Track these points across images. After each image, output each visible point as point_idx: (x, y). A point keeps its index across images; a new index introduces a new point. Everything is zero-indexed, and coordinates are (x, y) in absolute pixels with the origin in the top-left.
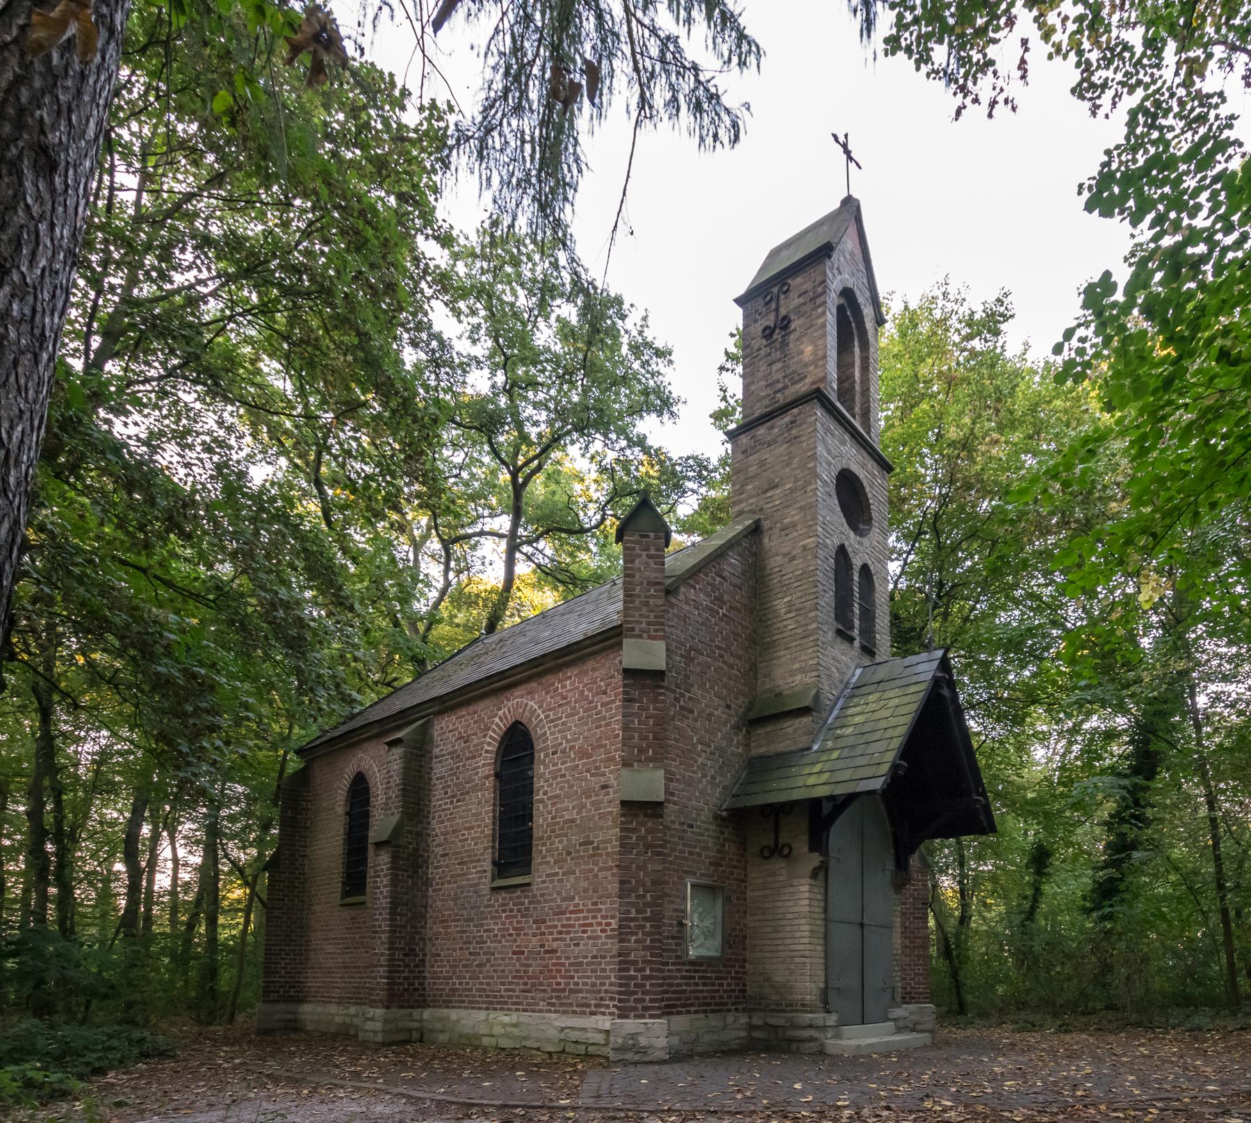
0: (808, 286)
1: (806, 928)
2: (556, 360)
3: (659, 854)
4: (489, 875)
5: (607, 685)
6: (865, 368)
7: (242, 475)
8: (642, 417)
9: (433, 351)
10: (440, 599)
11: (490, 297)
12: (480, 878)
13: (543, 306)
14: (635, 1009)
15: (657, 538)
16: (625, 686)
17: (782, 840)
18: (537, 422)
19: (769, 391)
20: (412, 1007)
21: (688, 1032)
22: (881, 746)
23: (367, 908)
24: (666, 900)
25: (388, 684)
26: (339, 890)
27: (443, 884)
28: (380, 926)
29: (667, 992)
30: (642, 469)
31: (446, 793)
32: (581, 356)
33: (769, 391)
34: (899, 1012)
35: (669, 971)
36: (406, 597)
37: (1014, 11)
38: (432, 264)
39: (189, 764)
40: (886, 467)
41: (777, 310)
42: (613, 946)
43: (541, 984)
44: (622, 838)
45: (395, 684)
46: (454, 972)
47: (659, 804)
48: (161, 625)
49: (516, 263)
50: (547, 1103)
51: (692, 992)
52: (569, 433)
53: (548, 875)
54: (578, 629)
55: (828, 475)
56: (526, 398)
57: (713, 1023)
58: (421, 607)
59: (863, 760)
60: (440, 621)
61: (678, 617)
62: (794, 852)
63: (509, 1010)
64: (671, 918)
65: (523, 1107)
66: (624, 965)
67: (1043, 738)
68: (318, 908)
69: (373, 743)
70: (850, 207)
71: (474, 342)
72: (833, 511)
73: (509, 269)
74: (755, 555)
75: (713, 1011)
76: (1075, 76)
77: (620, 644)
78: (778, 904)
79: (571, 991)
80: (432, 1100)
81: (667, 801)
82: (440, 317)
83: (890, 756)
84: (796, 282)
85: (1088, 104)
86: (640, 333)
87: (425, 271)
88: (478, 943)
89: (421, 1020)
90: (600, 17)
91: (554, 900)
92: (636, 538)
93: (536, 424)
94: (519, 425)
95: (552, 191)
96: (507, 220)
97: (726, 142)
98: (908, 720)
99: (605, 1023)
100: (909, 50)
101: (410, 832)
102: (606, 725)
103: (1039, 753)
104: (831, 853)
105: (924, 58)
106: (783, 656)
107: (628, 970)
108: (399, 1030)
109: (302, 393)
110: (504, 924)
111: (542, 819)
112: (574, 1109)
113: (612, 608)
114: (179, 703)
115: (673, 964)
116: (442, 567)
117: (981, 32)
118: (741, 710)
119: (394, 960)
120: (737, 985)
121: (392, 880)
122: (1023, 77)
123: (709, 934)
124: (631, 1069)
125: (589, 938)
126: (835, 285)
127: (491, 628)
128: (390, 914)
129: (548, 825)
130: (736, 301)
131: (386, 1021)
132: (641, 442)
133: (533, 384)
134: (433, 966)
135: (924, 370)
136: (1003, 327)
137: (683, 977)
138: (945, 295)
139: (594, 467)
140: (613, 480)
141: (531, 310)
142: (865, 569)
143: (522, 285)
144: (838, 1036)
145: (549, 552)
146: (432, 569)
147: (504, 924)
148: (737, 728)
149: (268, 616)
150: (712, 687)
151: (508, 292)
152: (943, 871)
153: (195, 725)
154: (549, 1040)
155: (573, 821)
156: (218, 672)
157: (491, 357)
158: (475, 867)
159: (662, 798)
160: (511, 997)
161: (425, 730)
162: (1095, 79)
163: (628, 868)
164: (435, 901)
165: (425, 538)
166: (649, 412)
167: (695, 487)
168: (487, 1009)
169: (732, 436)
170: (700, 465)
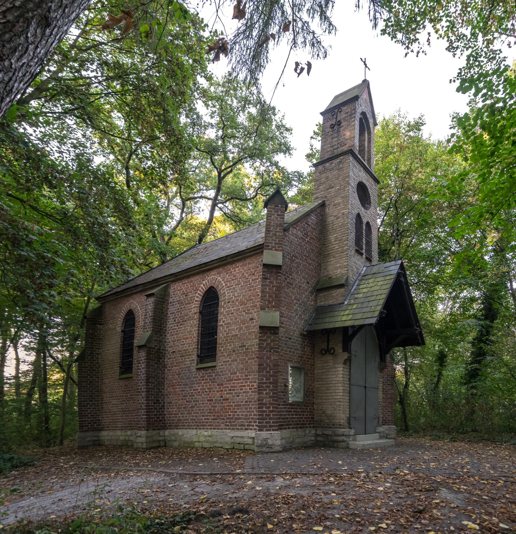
0: (349, 110)
1: (341, 388)
2: (245, 128)
3: (277, 352)
4: (195, 362)
5: (255, 271)
6: (369, 142)
7: (89, 161)
8: (277, 154)
9: (194, 119)
10: (177, 226)
11: (222, 101)
12: (191, 364)
13: (244, 108)
14: (266, 427)
15: (282, 207)
16: (263, 272)
17: (330, 346)
18: (233, 151)
19: (331, 149)
20: (159, 429)
21: (289, 438)
22: (375, 303)
23: (133, 380)
24: (279, 374)
25: (147, 265)
26: (118, 371)
27: (172, 367)
28: (141, 389)
29: (279, 418)
30: (275, 175)
31: (175, 321)
32: (255, 128)
33: (331, 149)
34: (381, 429)
35: (281, 408)
36: (161, 223)
37: (425, 24)
38: (201, 86)
39: (34, 303)
40: (377, 181)
41: (336, 118)
42: (256, 396)
43: (222, 416)
44: (259, 344)
45: (151, 265)
46: (179, 411)
47: (277, 328)
48: (29, 231)
49: (235, 90)
50: (231, 472)
51: (291, 418)
52: (246, 158)
53: (224, 362)
54: (243, 245)
55: (354, 184)
56: (230, 142)
57: (300, 433)
58: (166, 228)
59: (368, 309)
60: (176, 236)
61: (288, 241)
62: (336, 352)
63: (207, 429)
64: (281, 383)
65: (220, 474)
66: (261, 405)
67: (442, 300)
68: (107, 381)
69: (139, 295)
70: (366, 84)
71: (212, 117)
72: (355, 199)
73: (232, 92)
74: (322, 216)
75: (300, 428)
76: (447, 44)
77: (262, 252)
78: (329, 376)
79: (236, 418)
80: (177, 473)
81: (280, 326)
82: (200, 107)
83: (379, 308)
84: (344, 108)
85: (452, 53)
86: (281, 121)
87: (197, 89)
88: (190, 396)
89: (164, 436)
90: (283, 12)
91: (227, 374)
92: (273, 206)
93: (233, 153)
94: (225, 153)
95: (256, 68)
96: (235, 74)
97: (322, 57)
98: (387, 291)
99: (252, 434)
100: (389, 34)
101: (156, 340)
102: (254, 290)
103: (440, 307)
104: (352, 353)
105: (394, 37)
106: (332, 261)
107: (262, 408)
108: (154, 441)
109: (129, 129)
110: (203, 386)
111: (221, 335)
112: (243, 474)
113: (259, 236)
114: (31, 271)
115: (282, 405)
116: (180, 211)
117: (414, 29)
118: (313, 285)
119: (149, 406)
120: (310, 415)
121: (147, 365)
122: (429, 44)
123: (297, 391)
124: (265, 455)
125: (244, 392)
126: (359, 111)
127: (200, 240)
128: (146, 382)
129: (224, 337)
130: (321, 113)
131: (147, 437)
132: (276, 164)
133: (234, 137)
134: (168, 409)
135: (391, 143)
136: (422, 128)
137: (287, 411)
138: (399, 115)
139: (255, 173)
140: (262, 179)
141: (238, 108)
142: (368, 223)
143: (236, 98)
144: (355, 440)
145: (230, 207)
146: (176, 212)
147: (203, 386)
148: (312, 293)
149: (90, 228)
150: (301, 274)
151: (230, 100)
152: (397, 364)
153: (40, 283)
154: (226, 443)
155: (236, 335)
156: (58, 256)
157: (218, 124)
158: (189, 358)
159: (278, 325)
160: (207, 422)
161: (166, 289)
162: (454, 45)
163: (262, 358)
164: (168, 376)
165: (174, 197)
166: (280, 152)
167: (297, 184)
168: (196, 429)
169: (315, 165)
170: (299, 176)
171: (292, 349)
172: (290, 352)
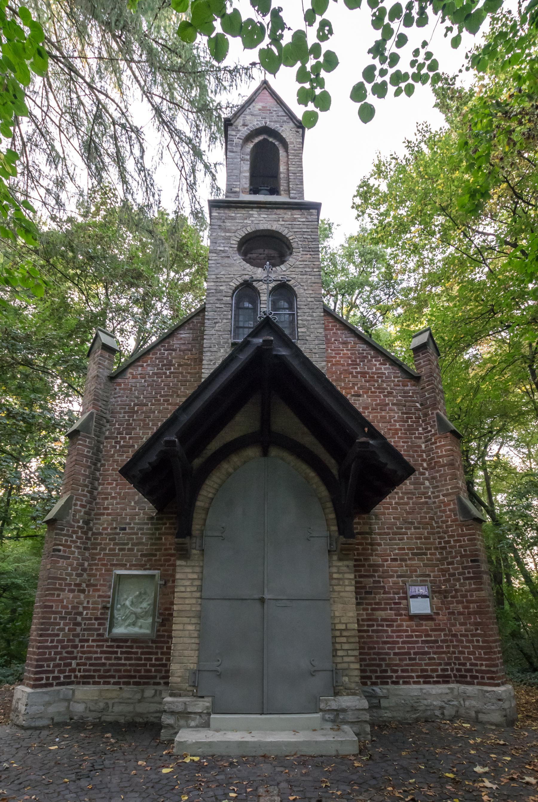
21: (96, 702)
57: (126, 695)
115: (93, 641)
171: (127, 544)
172: (121, 550)
